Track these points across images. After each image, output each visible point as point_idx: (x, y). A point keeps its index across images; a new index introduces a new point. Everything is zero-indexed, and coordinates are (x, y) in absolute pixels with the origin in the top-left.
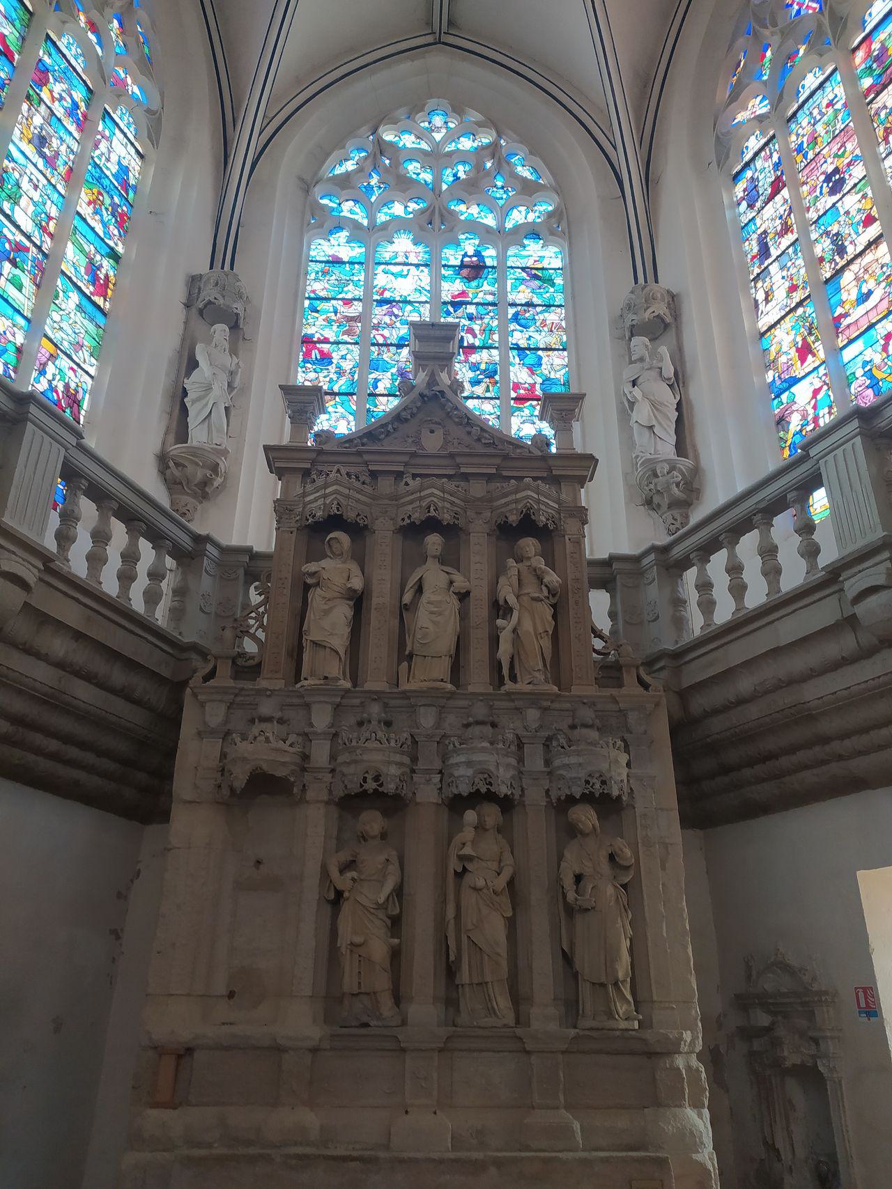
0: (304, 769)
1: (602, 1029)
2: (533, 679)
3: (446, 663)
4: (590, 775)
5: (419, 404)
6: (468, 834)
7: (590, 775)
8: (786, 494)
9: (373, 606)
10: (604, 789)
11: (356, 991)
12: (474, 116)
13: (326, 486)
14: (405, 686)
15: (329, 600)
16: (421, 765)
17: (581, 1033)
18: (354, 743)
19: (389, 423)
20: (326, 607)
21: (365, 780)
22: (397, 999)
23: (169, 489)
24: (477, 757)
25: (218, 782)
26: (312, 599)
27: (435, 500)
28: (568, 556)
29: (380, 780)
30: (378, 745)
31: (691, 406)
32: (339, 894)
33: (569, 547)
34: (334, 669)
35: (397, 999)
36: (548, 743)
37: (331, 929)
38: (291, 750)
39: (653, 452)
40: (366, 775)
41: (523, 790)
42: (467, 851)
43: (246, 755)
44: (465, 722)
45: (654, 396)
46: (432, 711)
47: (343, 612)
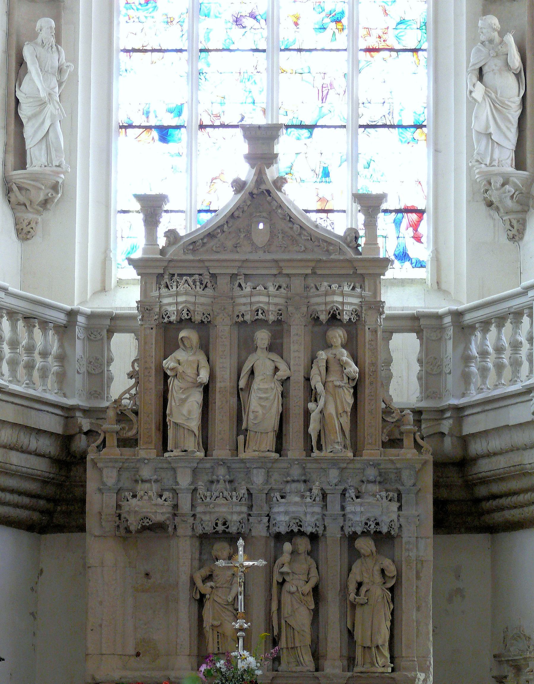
0: (175, 515)
1: (368, 673)
4: (367, 520)
5: (249, 203)
6: (285, 558)
7: (367, 520)
8: (524, 309)
9: (217, 390)
10: (377, 528)
11: (216, 651)
13: (177, 294)
14: (242, 455)
15: (185, 390)
16: (255, 511)
17: (356, 674)
18: (208, 499)
19: (224, 224)
20: (183, 397)
21: (217, 524)
23: (12, 209)
24: (293, 509)
25: (117, 523)
26: (172, 388)
27: (262, 305)
28: (367, 344)
29: (226, 524)
30: (225, 502)
32: (203, 596)
33: (368, 336)
36: (345, 493)
37: (199, 617)
38: (166, 503)
39: (488, 164)
40: (217, 521)
41: (325, 527)
42: (285, 569)
43: (137, 509)
44: (285, 480)
45: (496, 93)
46: (262, 472)
47: (197, 397)
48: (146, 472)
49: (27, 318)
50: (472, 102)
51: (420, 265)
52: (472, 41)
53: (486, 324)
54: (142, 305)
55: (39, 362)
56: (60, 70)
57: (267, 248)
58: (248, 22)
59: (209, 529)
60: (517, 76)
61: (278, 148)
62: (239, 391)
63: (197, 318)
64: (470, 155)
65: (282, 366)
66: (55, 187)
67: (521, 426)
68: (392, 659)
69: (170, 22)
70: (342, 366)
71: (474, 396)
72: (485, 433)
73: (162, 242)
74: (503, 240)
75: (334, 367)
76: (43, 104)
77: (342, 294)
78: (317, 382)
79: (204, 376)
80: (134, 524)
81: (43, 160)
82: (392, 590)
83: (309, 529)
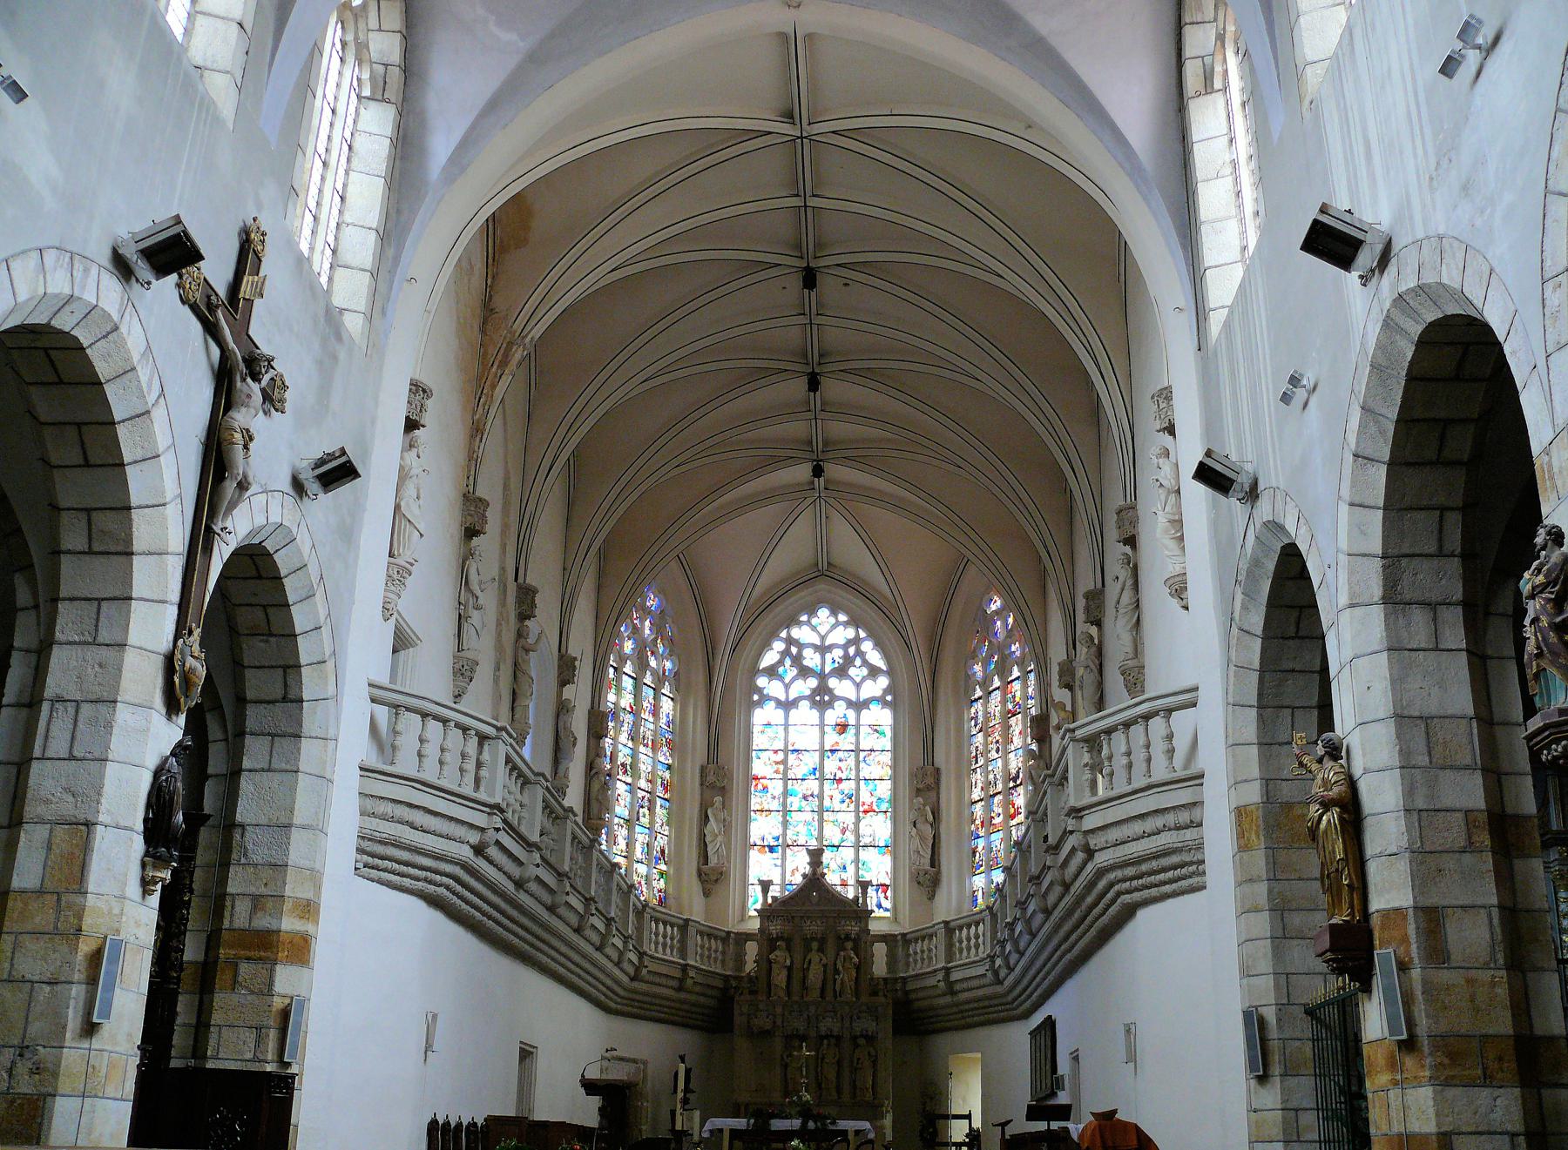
2: (849, 996)
3: (818, 991)
12: (842, 618)
31: (939, 837)
34: (782, 994)
47: (784, 973)
51: (887, 910)
52: (910, 809)
53: (916, 940)
54: (761, 930)
57: (818, 904)
63: (786, 935)
64: (910, 859)
66: (721, 874)
69: (774, 798)
70: (851, 958)
73: (770, 901)
74: (925, 898)
79: (788, 962)
83: (835, 1034)
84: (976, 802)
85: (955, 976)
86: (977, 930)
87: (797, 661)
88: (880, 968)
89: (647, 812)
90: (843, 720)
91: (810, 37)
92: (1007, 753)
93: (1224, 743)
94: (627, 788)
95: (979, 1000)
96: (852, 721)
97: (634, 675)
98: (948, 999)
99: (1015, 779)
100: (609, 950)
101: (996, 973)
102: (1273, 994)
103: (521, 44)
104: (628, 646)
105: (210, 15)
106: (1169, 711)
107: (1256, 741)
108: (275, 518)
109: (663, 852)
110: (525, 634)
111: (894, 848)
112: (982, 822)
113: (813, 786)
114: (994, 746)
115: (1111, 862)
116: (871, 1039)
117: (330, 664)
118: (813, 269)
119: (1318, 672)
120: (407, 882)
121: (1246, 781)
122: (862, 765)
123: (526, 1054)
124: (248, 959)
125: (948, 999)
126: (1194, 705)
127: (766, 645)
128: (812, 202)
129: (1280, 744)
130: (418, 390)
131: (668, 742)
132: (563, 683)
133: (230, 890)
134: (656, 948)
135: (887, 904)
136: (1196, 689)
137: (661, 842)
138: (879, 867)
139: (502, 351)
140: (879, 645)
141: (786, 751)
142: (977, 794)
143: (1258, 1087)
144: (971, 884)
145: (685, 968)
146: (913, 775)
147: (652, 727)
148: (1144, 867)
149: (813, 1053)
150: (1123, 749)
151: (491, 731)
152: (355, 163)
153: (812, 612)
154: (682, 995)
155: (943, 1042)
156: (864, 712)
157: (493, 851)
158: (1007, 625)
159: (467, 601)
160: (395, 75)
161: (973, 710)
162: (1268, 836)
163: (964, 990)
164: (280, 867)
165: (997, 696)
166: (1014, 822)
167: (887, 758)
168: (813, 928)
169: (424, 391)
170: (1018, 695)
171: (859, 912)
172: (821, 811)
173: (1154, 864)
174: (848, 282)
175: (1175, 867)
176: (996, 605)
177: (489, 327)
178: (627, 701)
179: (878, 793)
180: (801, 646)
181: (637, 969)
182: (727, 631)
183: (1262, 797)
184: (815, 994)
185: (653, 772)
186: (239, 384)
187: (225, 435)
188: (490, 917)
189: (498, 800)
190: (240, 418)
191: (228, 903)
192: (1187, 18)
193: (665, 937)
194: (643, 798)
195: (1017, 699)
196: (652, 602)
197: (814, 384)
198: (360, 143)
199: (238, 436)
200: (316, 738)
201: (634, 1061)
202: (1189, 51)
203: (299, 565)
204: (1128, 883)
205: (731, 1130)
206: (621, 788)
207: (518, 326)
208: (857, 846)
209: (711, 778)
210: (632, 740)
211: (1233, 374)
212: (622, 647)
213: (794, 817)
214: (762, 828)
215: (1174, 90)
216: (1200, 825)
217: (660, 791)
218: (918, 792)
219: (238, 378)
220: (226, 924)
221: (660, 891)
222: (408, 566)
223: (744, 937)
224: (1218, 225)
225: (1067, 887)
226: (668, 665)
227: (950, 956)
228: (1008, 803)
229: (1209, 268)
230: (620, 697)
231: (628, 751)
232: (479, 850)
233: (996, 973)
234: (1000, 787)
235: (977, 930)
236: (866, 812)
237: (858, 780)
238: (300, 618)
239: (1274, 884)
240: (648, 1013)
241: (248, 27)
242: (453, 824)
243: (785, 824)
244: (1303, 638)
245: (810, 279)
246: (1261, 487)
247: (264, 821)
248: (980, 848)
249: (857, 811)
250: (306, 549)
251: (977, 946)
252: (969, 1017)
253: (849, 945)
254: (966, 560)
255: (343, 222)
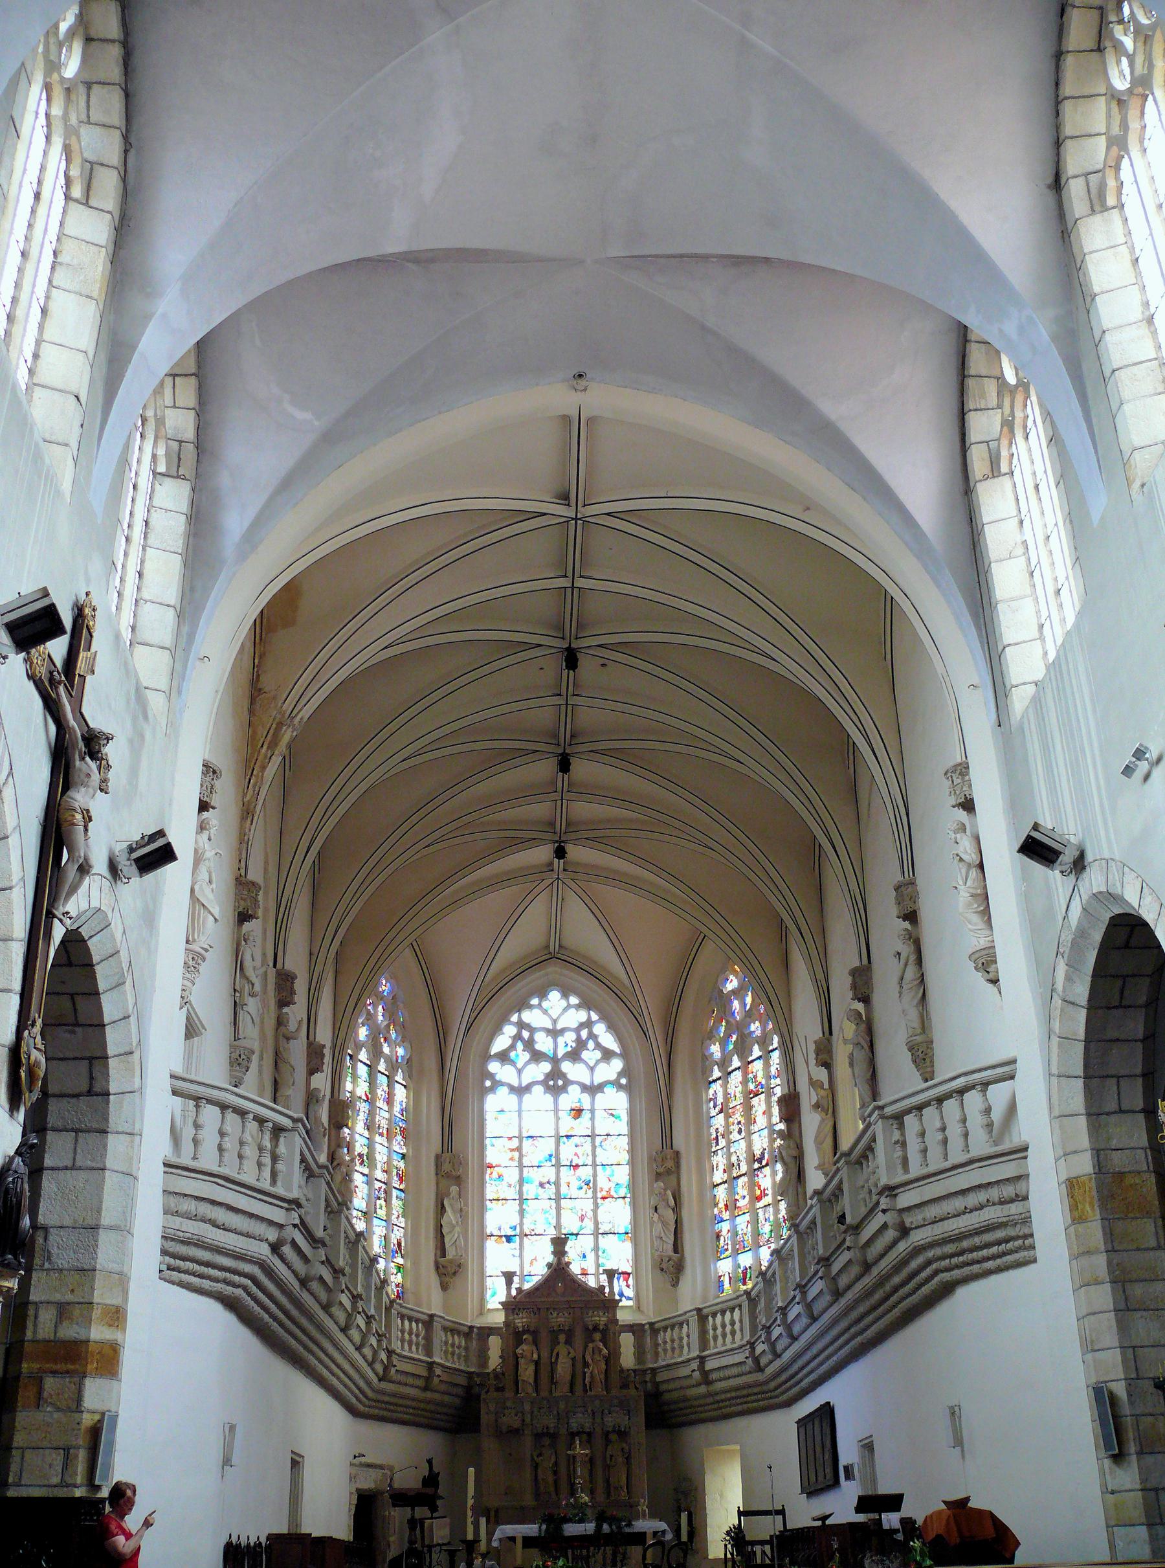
2: (599, 1389)
12: (574, 1000)
22: (557, 1494)
31: (682, 1224)
32: (537, 1464)
34: (530, 1389)
35: (557, 1494)
47: (532, 1368)
48: (509, 1404)
49: (452, 1331)
50: (652, 1223)
52: (651, 1192)
53: (665, 1329)
54: (506, 1324)
55: (457, 1351)
56: (461, 1210)
58: (547, 1186)
59: (540, 1431)
60: (673, 1210)
61: (567, 1248)
62: (551, 1363)
65: (572, 1351)
67: (685, 1377)
68: (628, 1492)
69: (510, 1186)
70: (600, 1351)
71: (661, 1363)
72: (668, 1381)
73: (514, 1293)
74: (668, 1286)
75: (596, 1351)
76: (454, 1227)
77: (599, 1316)
78: (588, 1358)
79: (535, 1356)
80: (504, 1429)
81: (454, 1253)
82: (627, 1458)
84: (718, 1185)
85: (709, 1366)
86: (723, 1318)
87: (529, 1044)
88: (627, 1359)
89: (383, 1204)
90: (578, 1105)
91: (591, 420)
92: (750, 1134)
93: (1046, 1111)
94: (365, 1179)
95: (737, 1389)
96: (586, 1105)
97: (368, 1063)
98: (703, 1389)
99: (760, 1160)
100: (367, 1351)
101: (756, 1360)
102: (1120, 1368)
103: (317, 423)
104: (363, 1033)
105: (47, 387)
106: (986, 1085)
107: (1083, 1111)
108: (95, 904)
109: (399, 1244)
110: (285, 1021)
111: (634, 1234)
112: (726, 1206)
113: (549, 1173)
114: (736, 1128)
115: (929, 1240)
116: (623, 1434)
117: (136, 1055)
118: (574, 649)
119: (1141, 1041)
120: (206, 1284)
121: (1075, 1152)
122: (599, 1150)
123: (296, 1464)
124: (54, 1373)
125: (703, 1389)
126: (1012, 1077)
127: (497, 1030)
128: (580, 583)
129: (1108, 1114)
130: (209, 770)
131: (402, 1131)
132: (311, 1072)
133: (32, 1298)
134: (417, 1349)
135: (629, 1292)
136: (1014, 1062)
137: (397, 1234)
138: (620, 1254)
139: (272, 731)
140: (612, 1027)
141: (520, 1138)
142: (718, 1177)
143: (1114, 1467)
144: (716, 1269)
145: (431, 1365)
146: (652, 1159)
147: (387, 1115)
148: (965, 1244)
149: (587, 1452)
150: (938, 1124)
151: (286, 1122)
152: (152, 540)
153: (543, 995)
154: (429, 1395)
155: (696, 1435)
156: (599, 1096)
157: (287, 1250)
158: (745, 1005)
159: (242, 989)
160: (190, 450)
161: (711, 1092)
162: (1103, 1206)
163: (720, 1380)
164: (87, 1272)
165: (737, 1077)
166: (759, 1205)
167: (624, 1142)
168: (559, 1319)
169: (214, 772)
170: (760, 1075)
171: (610, 1305)
172: (558, 1198)
173: (977, 1240)
174: (606, 662)
175: (999, 1243)
176: (732, 984)
177: (257, 706)
178: (362, 1089)
179: (615, 1179)
180: (532, 1030)
181: (386, 1368)
182: (458, 1012)
183: (1094, 1167)
184: (562, 1390)
185: (389, 1162)
186: (78, 763)
187: (66, 815)
188: (275, 1319)
189: (294, 1194)
190: (80, 797)
191: (31, 1312)
192: (970, 404)
193: (410, 1333)
194: (380, 1188)
195: (759, 1079)
196: (385, 987)
197: (564, 765)
198: (156, 518)
199: (79, 817)
200: (122, 1133)
201: (381, 1467)
202: (973, 436)
203: (111, 951)
204: (947, 1261)
205: (523, 1537)
206: (358, 1179)
207: (288, 706)
208: (596, 1233)
209: (447, 1167)
210: (368, 1129)
211: (1046, 748)
212: (357, 1034)
213: (530, 1206)
214: (498, 1218)
215: (960, 475)
216: (1026, 1198)
217: (395, 1182)
218: (658, 1176)
219: (77, 757)
220: (29, 1335)
221: (397, 1286)
222: (203, 952)
223: (489, 1331)
224: (1014, 604)
225: (867, 1267)
226: (401, 1051)
227: (704, 1345)
228: (753, 1185)
229: (1009, 645)
230: (356, 1085)
231: (366, 1142)
232: (275, 1248)
233: (756, 1360)
234: (744, 1168)
235: (723, 1318)
236: (604, 1198)
237: (594, 1165)
238: (110, 1008)
239: (1113, 1255)
240: (395, 1415)
241: (83, 399)
242: (253, 1221)
243: (522, 1212)
244: (1125, 1007)
245: (571, 659)
246: (1089, 857)
247: (67, 1222)
248: (724, 1233)
249: (595, 1198)
250: (118, 935)
251: (733, 1333)
252: (727, 1407)
253: (597, 1336)
254: (702, 935)
255: (141, 599)
